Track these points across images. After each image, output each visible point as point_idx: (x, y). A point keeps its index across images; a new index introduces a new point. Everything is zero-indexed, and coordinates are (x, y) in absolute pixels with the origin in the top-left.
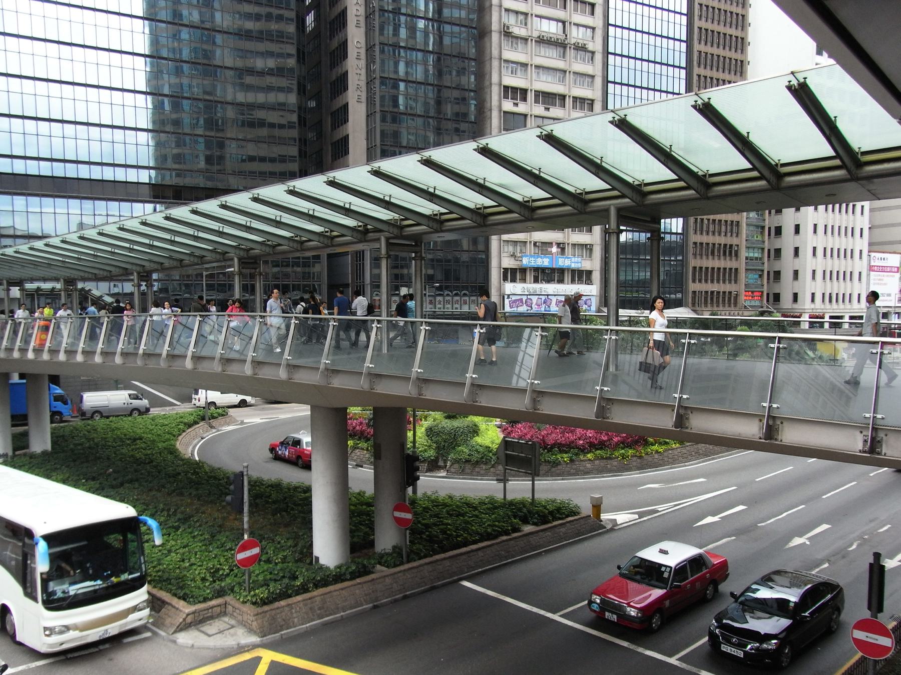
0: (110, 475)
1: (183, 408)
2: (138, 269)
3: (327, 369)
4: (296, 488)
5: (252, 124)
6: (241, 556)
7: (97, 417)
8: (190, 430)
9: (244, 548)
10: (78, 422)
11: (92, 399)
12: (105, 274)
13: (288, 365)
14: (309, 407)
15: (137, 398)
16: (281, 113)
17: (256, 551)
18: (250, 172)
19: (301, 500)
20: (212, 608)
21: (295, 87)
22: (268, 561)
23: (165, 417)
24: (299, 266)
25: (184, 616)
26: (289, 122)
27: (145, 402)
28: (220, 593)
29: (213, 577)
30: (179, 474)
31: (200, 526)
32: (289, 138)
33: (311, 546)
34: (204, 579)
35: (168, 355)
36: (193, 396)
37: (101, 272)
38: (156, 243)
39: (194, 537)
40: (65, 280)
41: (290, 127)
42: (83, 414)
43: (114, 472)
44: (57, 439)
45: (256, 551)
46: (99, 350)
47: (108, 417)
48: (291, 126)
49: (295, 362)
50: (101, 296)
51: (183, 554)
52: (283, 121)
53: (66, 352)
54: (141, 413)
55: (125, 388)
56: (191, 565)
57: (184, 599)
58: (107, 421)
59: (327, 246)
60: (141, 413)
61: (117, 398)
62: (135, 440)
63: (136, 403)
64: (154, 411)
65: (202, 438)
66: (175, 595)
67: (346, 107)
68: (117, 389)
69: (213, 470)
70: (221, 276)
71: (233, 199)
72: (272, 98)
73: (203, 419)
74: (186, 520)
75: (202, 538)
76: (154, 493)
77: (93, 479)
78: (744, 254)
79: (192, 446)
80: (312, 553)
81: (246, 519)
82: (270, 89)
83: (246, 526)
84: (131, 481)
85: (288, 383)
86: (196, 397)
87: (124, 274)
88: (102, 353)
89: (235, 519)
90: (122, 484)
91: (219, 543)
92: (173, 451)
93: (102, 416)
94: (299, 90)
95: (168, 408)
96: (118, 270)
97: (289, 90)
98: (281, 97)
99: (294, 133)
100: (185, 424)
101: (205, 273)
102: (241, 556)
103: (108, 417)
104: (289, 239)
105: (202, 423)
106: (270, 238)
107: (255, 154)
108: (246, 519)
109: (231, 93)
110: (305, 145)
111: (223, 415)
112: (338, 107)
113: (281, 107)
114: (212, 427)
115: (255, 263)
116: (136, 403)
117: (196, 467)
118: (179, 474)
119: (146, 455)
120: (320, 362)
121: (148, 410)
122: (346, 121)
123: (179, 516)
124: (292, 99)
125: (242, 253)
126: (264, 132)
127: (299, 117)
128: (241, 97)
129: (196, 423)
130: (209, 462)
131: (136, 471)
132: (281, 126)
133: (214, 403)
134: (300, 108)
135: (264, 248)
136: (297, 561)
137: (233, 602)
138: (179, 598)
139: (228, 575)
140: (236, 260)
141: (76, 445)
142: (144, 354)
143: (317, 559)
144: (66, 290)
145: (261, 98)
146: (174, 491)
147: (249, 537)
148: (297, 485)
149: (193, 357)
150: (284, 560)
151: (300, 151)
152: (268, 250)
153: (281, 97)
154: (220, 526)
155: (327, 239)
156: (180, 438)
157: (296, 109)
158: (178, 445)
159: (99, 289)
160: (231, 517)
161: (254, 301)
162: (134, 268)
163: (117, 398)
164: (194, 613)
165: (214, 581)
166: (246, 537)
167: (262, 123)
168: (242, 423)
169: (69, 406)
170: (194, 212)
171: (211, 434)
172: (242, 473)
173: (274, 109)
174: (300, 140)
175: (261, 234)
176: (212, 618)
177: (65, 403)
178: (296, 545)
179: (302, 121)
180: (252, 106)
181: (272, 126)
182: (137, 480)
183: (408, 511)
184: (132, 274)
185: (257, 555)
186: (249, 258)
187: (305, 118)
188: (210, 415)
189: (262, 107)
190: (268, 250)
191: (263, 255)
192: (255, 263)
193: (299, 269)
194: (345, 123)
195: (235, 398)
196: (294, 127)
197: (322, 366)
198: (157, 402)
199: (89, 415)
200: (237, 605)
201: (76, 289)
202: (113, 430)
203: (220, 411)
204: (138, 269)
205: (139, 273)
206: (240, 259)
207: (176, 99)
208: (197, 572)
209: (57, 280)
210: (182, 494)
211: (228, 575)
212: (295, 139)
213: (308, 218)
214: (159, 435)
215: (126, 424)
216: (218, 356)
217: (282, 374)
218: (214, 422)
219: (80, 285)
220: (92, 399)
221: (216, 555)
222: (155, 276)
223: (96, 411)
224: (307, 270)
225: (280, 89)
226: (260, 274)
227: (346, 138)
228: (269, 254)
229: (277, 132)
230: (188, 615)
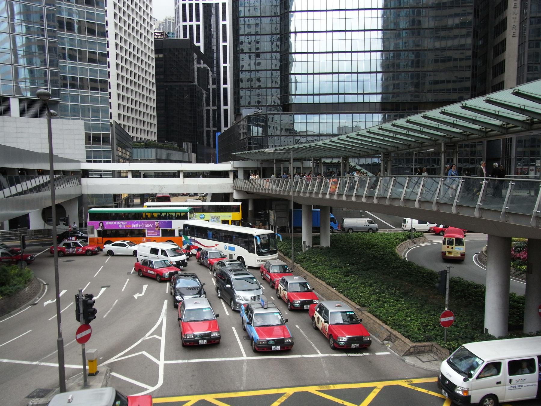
0: (361, 263)
1: (396, 230)
2: (384, 151)
3: (506, 213)
4: (470, 285)
5: (443, 61)
6: (443, 320)
7: (350, 231)
8: (402, 243)
9: (445, 315)
10: (340, 233)
11: (349, 221)
12: (365, 154)
13: (480, 209)
14: (486, 236)
15: (371, 223)
16: (462, 51)
17: (451, 318)
18: (440, 90)
19: (474, 292)
20: (424, 346)
21: (472, 34)
22: (456, 326)
23: (388, 234)
24: (468, 147)
25: (409, 347)
26: (466, 57)
27: (376, 225)
28: (428, 339)
29: (424, 329)
30: (399, 267)
31: (414, 298)
32: (466, 66)
33: (483, 321)
34: (419, 329)
35: (404, 199)
36: (403, 224)
37: (363, 153)
38: (397, 136)
39: (411, 304)
40: (343, 157)
41: (467, 59)
42: (343, 229)
43: (364, 262)
44: (333, 241)
45: (451, 318)
46: (354, 194)
47: (357, 232)
48: (467, 58)
49: (485, 207)
50: (355, 166)
51: (408, 312)
52: (462, 56)
53: (346, 195)
54: (373, 231)
55: (365, 217)
56: (412, 320)
57: (408, 338)
58: (357, 234)
59: (504, 134)
60: (373, 231)
61: (360, 222)
62: (373, 246)
63: (371, 225)
64: (381, 231)
65: (409, 249)
66: (403, 335)
67: (504, 42)
68: (361, 217)
69: (419, 267)
70: (421, 154)
71: (449, 108)
72: (456, 42)
73: (409, 237)
74: (406, 294)
75: (416, 306)
76: (386, 276)
77: (353, 264)
78: (59, 78)
79: (404, 251)
80: (483, 326)
81: (447, 299)
82: (456, 37)
83: (447, 303)
84: (373, 268)
85: (479, 219)
86: (404, 224)
87: (374, 153)
88: (366, 197)
89: (434, 298)
90: (368, 269)
91: (426, 310)
92: (395, 255)
93: (353, 232)
94: (474, 35)
95: (388, 230)
96: (373, 152)
97: (468, 35)
98: (462, 41)
99: (470, 63)
100: (400, 239)
101: (414, 153)
102: (443, 320)
103: (357, 232)
104: (479, 130)
105: (409, 240)
106: (467, 130)
107: (445, 79)
108: (447, 299)
109: (428, 43)
110: (476, 70)
111: (420, 236)
112: (498, 42)
113: (462, 47)
114: (414, 243)
115: (454, 146)
116: (371, 225)
117: (408, 265)
118: (399, 267)
119: (381, 254)
120: (501, 208)
121: (377, 230)
122: (504, 50)
123: (403, 291)
124: (469, 41)
125: (447, 140)
126: (451, 64)
127: (473, 52)
128: (437, 44)
129: (405, 239)
130: (416, 263)
131: (375, 263)
132: (461, 60)
133: (414, 229)
134: (474, 47)
135: (461, 137)
136: (474, 329)
137: (436, 346)
138: (406, 337)
139: (433, 329)
140: (443, 144)
141: (343, 245)
142: (390, 198)
143: (487, 330)
144: (343, 163)
145: (450, 43)
146: (397, 277)
147: (449, 309)
148: (471, 283)
149: (419, 201)
150: (466, 326)
151: (473, 74)
152: (464, 137)
153: (462, 41)
154: (425, 301)
155: (504, 130)
156: (397, 247)
157: (471, 48)
158: (397, 251)
159: (353, 162)
160: (431, 297)
161: (440, 168)
162: (382, 150)
163: (360, 222)
164: (414, 347)
165: (425, 332)
166: (446, 309)
167: (449, 59)
168: (432, 242)
169: (337, 224)
170: (424, 117)
171: (413, 247)
172: (446, 271)
173: (457, 49)
174: (473, 67)
175: (461, 128)
176: (424, 352)
177: (335, 223)
178: (472, 320)
179: (475, 55)
180: (443, 50)
181: (456, 60)
182: (376, 268)
183: (445, 323)
184: (380, 154)
185: (451, 321)
186: (451, 143)
187: (477, 53)
188: (413, 235)
189: (450, 49)
190: (464, 137)
191: (460, 141)
192: (454, 146)
193: (468, 149)
194: (503, 52)
195: (428, 226)
196: (470, 59)
197: (503, 211)
198: (386, 227)
199: (346, 230)
200: (439, 348)
201: (321, 163)
202: (361, 239)
203: (419, 234)
204: (384, 151)
205: (384, 153)
206: (445, 144)
207: (397, 52)
208: (415, 324)
209: (339, 157)
210: (402, 279)
211: (433, 329)
212: (470, 66)
213: (494, 117)
214: (386, 244)
215: (367, 236)
216: (435, 201)
217: (476, 214)
218: (416, 240)
219: (323, 160)
220: (349, 221)
221: (425, 317)
222: (392, 155)
223: (351, 229)
224: (473, 149)
225: (462, 36)
226: (457, 152)
227: (504, 62)
228: (465, 140)
229: (459, 63)
230: (411, 347)
